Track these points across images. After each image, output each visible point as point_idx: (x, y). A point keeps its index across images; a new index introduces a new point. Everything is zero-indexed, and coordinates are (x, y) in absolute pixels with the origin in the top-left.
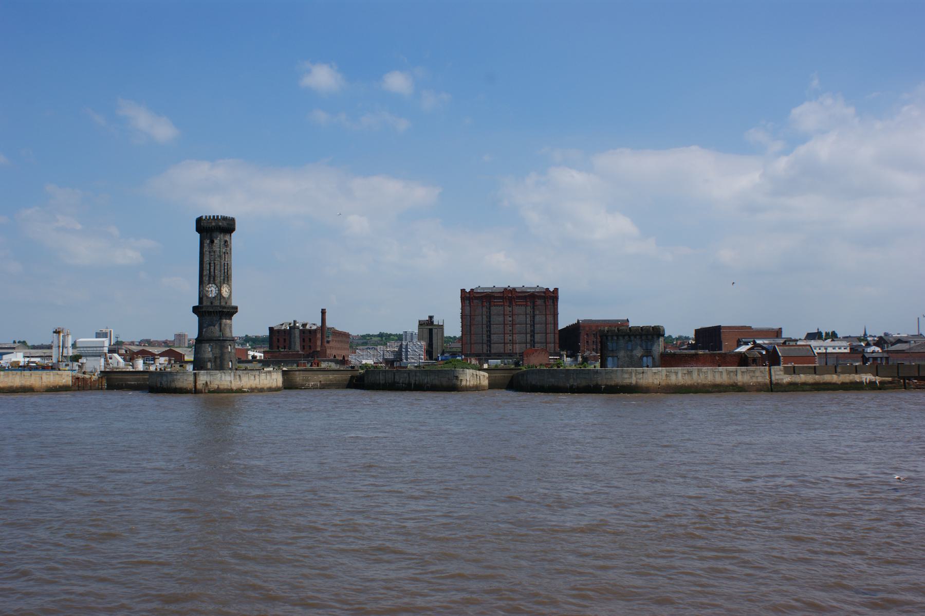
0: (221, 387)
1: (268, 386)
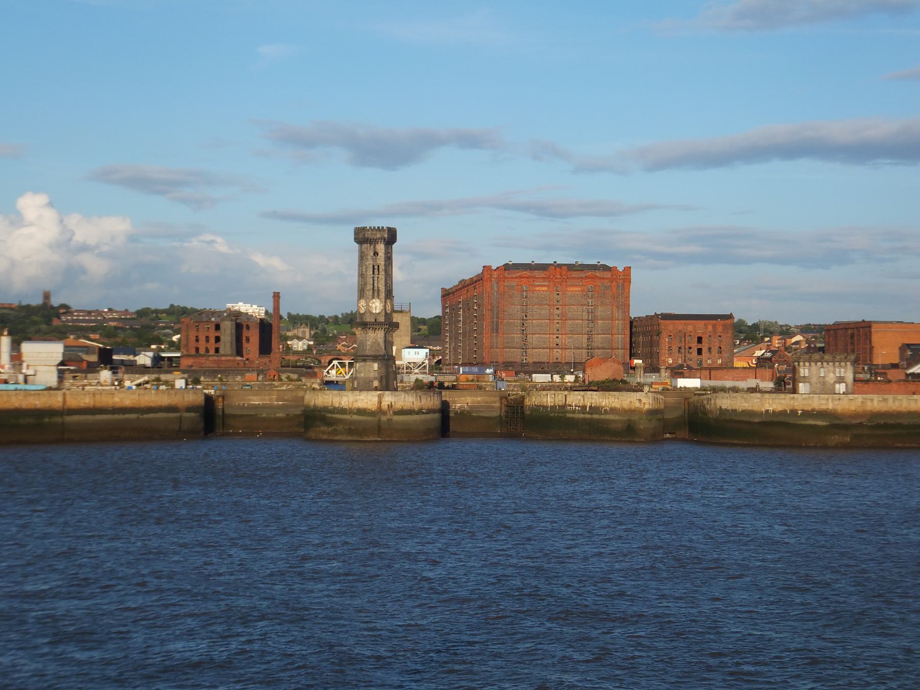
0: (405, 408)
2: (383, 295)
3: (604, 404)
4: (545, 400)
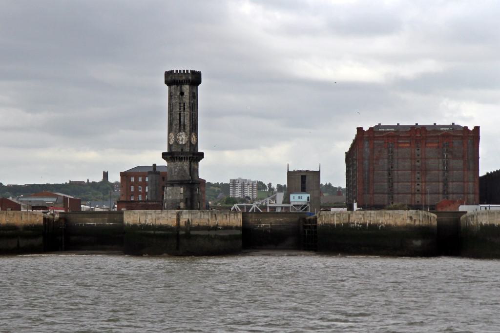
0: (201, 224)
1: (235, 225)
2: (188, 129)
3: (380, 222)
4: (332, 219)
